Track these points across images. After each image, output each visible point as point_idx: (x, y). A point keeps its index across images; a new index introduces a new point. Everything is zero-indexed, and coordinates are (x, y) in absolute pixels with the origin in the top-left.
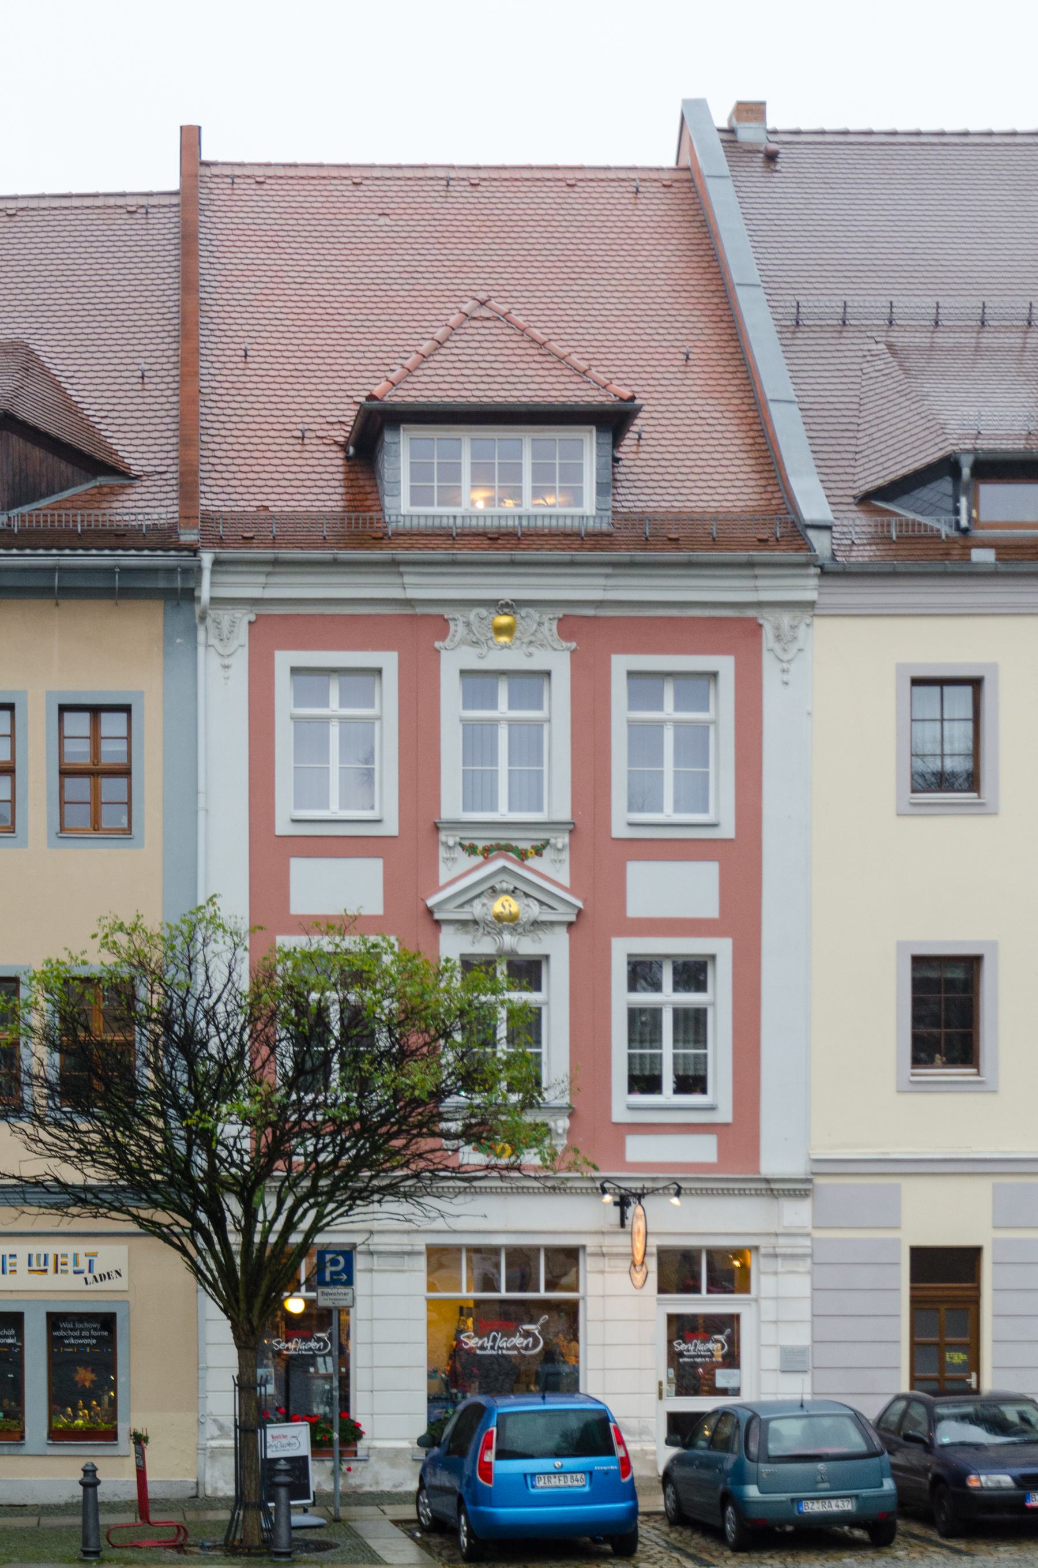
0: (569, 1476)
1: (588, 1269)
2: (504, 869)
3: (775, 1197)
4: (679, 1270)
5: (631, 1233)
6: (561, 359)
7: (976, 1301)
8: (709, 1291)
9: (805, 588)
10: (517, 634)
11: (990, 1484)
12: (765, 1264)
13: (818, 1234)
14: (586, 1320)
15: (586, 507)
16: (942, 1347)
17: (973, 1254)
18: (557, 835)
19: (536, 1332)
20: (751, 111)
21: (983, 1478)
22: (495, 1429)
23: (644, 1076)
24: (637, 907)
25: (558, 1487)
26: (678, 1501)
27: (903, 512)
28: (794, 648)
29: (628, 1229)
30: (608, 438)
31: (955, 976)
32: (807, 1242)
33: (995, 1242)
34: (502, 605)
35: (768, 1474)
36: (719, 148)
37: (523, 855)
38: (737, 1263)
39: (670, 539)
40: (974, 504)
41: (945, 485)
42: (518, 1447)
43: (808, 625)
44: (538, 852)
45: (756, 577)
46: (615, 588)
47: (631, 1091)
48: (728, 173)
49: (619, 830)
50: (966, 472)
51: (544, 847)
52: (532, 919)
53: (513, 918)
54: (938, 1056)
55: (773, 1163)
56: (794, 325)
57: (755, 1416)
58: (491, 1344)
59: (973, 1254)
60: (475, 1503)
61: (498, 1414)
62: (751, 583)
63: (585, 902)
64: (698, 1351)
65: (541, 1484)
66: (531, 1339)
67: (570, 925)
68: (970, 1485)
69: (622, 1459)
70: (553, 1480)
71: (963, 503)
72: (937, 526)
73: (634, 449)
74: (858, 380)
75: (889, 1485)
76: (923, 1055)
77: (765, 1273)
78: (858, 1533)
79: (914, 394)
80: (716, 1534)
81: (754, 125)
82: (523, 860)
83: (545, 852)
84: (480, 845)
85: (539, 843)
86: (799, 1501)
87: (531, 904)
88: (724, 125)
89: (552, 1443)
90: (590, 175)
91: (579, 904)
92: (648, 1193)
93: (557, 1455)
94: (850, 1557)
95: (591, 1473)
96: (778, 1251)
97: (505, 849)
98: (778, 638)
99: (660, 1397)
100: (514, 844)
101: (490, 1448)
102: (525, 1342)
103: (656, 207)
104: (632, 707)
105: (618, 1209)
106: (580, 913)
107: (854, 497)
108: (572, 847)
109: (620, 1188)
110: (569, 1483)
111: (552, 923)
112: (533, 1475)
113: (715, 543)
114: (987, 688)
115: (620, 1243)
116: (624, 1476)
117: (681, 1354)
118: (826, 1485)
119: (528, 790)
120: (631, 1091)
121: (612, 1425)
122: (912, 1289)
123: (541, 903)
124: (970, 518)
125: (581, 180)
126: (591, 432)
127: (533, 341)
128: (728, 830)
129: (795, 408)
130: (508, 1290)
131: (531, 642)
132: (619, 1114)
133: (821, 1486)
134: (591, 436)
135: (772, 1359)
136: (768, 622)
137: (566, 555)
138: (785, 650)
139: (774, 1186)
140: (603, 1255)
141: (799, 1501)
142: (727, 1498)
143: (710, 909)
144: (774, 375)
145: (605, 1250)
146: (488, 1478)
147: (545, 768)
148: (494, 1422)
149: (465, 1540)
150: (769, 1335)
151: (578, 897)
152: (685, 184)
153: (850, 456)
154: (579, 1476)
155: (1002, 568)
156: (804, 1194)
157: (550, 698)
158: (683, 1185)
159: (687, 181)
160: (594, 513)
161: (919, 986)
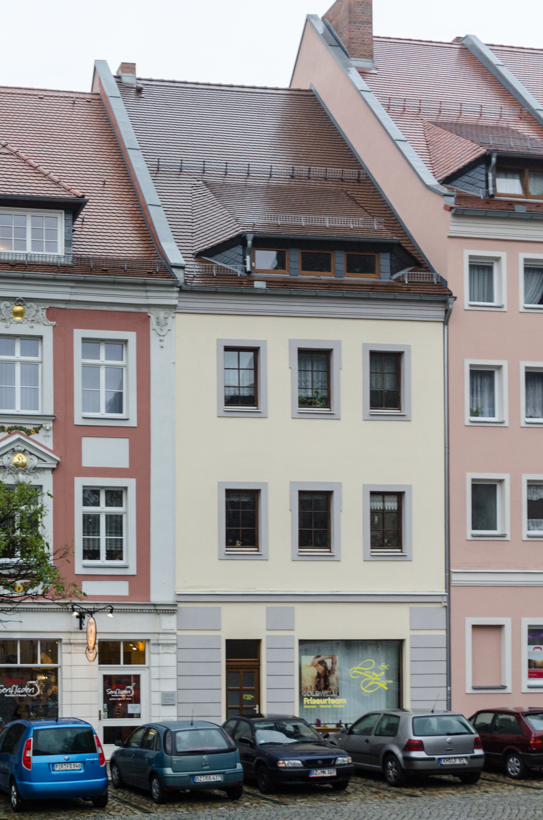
0: (72, 764)
1: (63, 651)
2: (19, 440)
3: (158, 614)
4: (108, 652)
5: (86, 632)
6: (46, 175)
7: (257, 668)
8: (124, 663)
9: (171, 298)
10: (25, 316)
11: (290, 765)
12: (153, 649)
13: (180, 633)
14: (62, 678)
15: (58, 252)
16: (241, 692)
17: (258, 642)
18: (47, 422)
19: (36, 685)
20: (128, 67)
21: (286, 762)
22: (32, 738)
23: (90, 550)
24: (88, 461)
25: (66, 770)
26: (120, 775)
27: (217, 262)
28: (166, 328)
29: (84, 630)
30: (70, 217)
31: (246, 500)
32: (174, 637)
33: (268, 637)
34: (18, 300)
35: (177, 761)
36: (115, 85)
37: (29, 433)
38: (134, 649)
39: (103, 270)
40: (253, 260)
41: (239, 250)
42: (44, 749)
43: (173, 317)
44: (37, 431)
45: (147, 291)
46: (76, 294)
47: (84, 558)
48: (120, 95)
49: (78, 421)
50: (249, 243)
51: (39, 428)
52: (34, 466)
53: (24, 465)
54: (238, 541)
55: (158, 595)
56: (156, 171)
57: (168, 730)
58: (12, 691)
59: (258, 642)
60: (22, 779)
61: (34, 730)
62: (144, 294)
63: (61, 457)
64: (119, 694)
65: (58, 769)
66: (33, 689)
67: (53, 470)
68: (280, 766)
69: (100, 754)
70: (64, 766)
71: (248, 258)
72: (235, 270)
73: (80, 226)
74: (190, 198)
75: (239, 766)
76: (230, 541)
77: (153, 653)
78: (216, 792)
79: (220, 205)
80: (147, 794)
81: (130, 75)
82: (29, 435)
83: (40, 431)
84: (7, 426)
85: (37, 426)
86: (193, 776)
87: (33, 458)
88: (115, 74)
89: (59, 746)
90: (50, 94)
91: (58, 459)
92: (97, 611)
93: (66, 753)
94: (222, 806)
95: (84, 762)
96: (160, 642)
97: (19, 429)
98: (158, 323)
99: (100, 719)
100: (24, 426)
101: (29, 749)
102: (30, 690)
103: (82, 112)
104: (83, 357)
105: (78, 620)
106: (58, 464)
107: (193, 254)
108: (54, 428)
109: (82, 608)
110: (73, 768)
111: (44, 469)
112: (53, 764)
113: (126, 273)
114: (262, 352)
115: (80, 637)
116: (102, 764)
117: (110, 696)
118: (208, 767)
119: (31, 397)
120: (84, 558)
121: (94, 735)
122: (227, 661)
123: (39, 458)
124: (252, 267)
125: (46, 96)
126: (61, 213)
127: (31, 166)
128: (133, 422)
129: (161, 209)
130: (21, 663)
131: (33, 321)
132: (79, 570)
133: (205, 768)
134: (62, 216)
135: (157, 698)
136: (153, 314)
137: (51, 275)
138: (161, 330)
139: (158, 608)
140: (71, 644)
141: (193, 776)
142: (154, 774)
143: (124, 463)
144: (149, 192)
145: (72, 641)
146: (28, 766)
147: (40, 387)
148: (32, 734)
149: (15, 800)
150: (155, 685)
151: (57, 456)
152: (97, 102)
153: (190, 234)
154: (78, 764)
155: (269, 292)
156: (173, 612)
157: (42, 350)
158: (115, 607)
159: (98, 100)
160: (63, 255)
161: (230, 505)
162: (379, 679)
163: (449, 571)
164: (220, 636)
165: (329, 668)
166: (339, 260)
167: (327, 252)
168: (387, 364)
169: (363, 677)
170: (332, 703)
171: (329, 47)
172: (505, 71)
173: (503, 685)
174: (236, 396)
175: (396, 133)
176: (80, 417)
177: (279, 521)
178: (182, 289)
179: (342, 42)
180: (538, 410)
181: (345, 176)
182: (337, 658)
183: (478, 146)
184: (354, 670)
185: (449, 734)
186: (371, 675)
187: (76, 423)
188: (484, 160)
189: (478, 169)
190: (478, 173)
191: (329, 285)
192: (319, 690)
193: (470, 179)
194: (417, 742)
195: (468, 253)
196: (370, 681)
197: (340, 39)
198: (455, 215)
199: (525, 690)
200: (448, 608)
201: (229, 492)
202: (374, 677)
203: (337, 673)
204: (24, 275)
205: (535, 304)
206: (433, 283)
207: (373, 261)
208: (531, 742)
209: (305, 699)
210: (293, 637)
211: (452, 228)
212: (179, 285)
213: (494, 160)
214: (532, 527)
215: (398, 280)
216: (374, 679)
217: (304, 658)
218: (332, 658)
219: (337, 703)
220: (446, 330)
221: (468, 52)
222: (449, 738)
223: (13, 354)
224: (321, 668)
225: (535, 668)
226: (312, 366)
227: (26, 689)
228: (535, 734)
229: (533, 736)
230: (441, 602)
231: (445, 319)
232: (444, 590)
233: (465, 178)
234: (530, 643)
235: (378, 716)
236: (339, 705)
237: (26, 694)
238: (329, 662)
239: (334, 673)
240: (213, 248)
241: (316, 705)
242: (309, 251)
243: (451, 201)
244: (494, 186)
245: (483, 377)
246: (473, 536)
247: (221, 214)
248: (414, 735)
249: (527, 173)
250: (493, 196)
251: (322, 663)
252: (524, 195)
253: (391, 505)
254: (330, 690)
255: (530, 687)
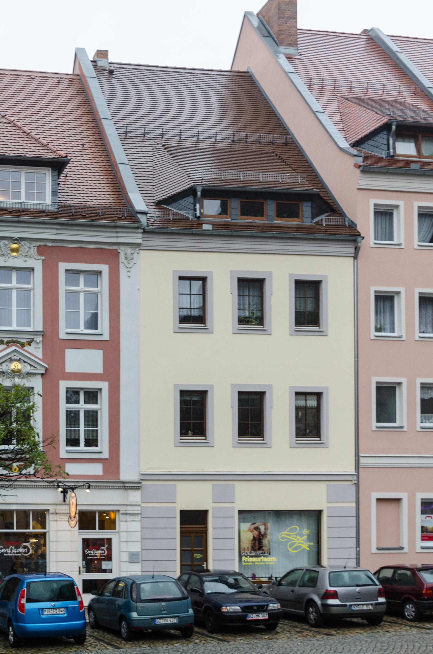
0: (58, 609)
1: (51, 519)
2: (15, 351)
3: (126, 489)
4: (86, 520)
5: (69, 504)
6: (36, 140)
7: (205, 532)
8: (99, 529)
9: (137, 238)
10: (20, 252)
11: (231, 610)
12: (122, 517)
13: (143, 505)
14: (49, 541)
15: (47, 201)
16: (192, 552)
17: (206, 512)
18: (37, 337)
19: (29, 546)
20: (102, 54)
21: (228, 608)
22: (25, 589)
23: (71, 439)
24: (70, 368)
25: (53, 614)
26: (95, 618)
27: (173, 209)
28: (132, 262)
29: (67, 503)
30: (56, 173)
31: (196, 399)
32: (139, 508)
33: (213, 508)
34: (14, 239)
35: (141, 607)
36: (92, 67)
37: (23, 345)
38: (107, 517)
39: (82, 215)
40: (202, 207)
41: (190, 199)
42: (35, 598)
43: (138, 253)
44: (29, 344)
45: (117, 232)
46: (60, 234)
47: (67, 445)
48: (95, 76)
49: (62, 336)
50: (199, 193)
51: (31, 342)
52: (27, 372)
53: (19, 371)
54: (190, 432)
55: (126, 475)
56: (125, 136)
57: (134, 582)
58: (10, 551)
59: (206, 512)
60: (17, 622)
61: (27, 582)
62: (115, 235)
63: (48, 365)
64: (95, 553)
65: (46, 613)
66: (26, 549)
67: (42, 375)
68: (223, 611)
69: (80, 601)
70: (51, 611)
71: (198, 206)
72: (187, 215)
73: (64, 180)
74: (152, 158)
75: (191, 611)
76: (184, 431)
77: (122, 521)
78: (173, 631)
79: (175, 163)
80: (117, 633)
81: (104, 60)
82: (23, 347)
83: (32, 344)
84: (5, 340)
85: (29, 340)
86: (154, 619)
87: (26, 366)
88: (92, 59)
89: (47, 595)
90: (40, 75)
91: (46, 366)
92: (77, 487)
93: (53, 601)
94: (177, 643)
95: (67, 608)
96: (128, 512)
97: (15, 342)
98: (126, 258)
99: (80, 574)
100: (19, 340)
101: (23, 597)
102: (24, 550)
103: (66, 90)
104: (67, 285)
105: (62, 494)
106: (46, 370)
107: (154, 203)
108: (43, 341)
109: (66, 485)
110: (58, 613)
111: (35, 374)
112: (42, 609)
113: (100, 218)
114: (209, 281)
115: (64, 508)
116: (81, 609)
117: (88, 555)
118: (166, 612)
119: (25, 317)
120: (67, 445)
121: (75, 587)
122: (181, 527)
123: (31, 365)
124: (201, 213)
125: (36, 76)
126: (49, 170)
127: (25, 132)
128: (106, 337)
129: (129, 167)
130: (17, 529)
131: (26, 256)
132: (63, 454)
133: (163, 612)
134: (49, 172)
135: (125, 557)
136: (122, 251)
137: (40, 220)
138: (129, 263)
139: (126, 485)
140: (57, 514)
141: (154, 619)
142: (123, 618)
143: (99, 369)
144: (119, 153)
145: (57, 511)
146: (23, 611)
147: (32, 309)
148: (25, 585)
149: (12, 638)
150: (124, 547)
151: (46, 363)
152: (78, 81)
153: (152, 187)
154: (62, 609)
155: (215, 233)
156: (138, 488)
157: (34, 279)
158: (91, 484)
159: (78, 79)
160: (51, 203)
161: (183, 403)
162: (302, 542)
163: (358, 455)
164: (175, 507)
165: (263, 533)
166: (270, 207)
167: (261, 201)
168: (308, 291)
169: (290, 540)
170: (265, 561)
171: (263, 38)
172: (403, 57)
173: (401, 546)
174: (188, 316)
175: (316, 106)
176: (64, 333)
177: (222, 415)
178: (145, 231)
179: (272, 34)
180: (429, 327)
181: (275, 141)
182: (269, 525)
183: (381, 116)
184: (282, 534)
185: (358, 586)
186: (296, 538)
187: (60, 337)
188: (386, 127)
189: (381, 135)
190: (381, 138)
191: (262, 227)
192: (254, 551)
193: (375, 142)
194: (332, 592)
195: (373, 201)
196: (295, 543)
197: (271, 31)
198: (363, 172)
199: (419, 550)
200: (357, 485)
201: (183, 393)
202: (298, 540)
203: (269, 537)
204: (19, 219)
205: (426, 242)
206: (346, 226)
207: (297, 208)
208: (424, 592)
209: (243, 557)
210: (233, 508)
211: (360, 182)
212: (143, 228)
213: (394, 127)
214: (424, 421)
215: (317, 223)
216: (298, 541)
217: (242, 525)
218: (265, 525)
219: (269, 561)
220: (356, 263)
221: (373, 42)
222: (358, 589)
223: (10, 282)
224: (256, 533)
225: (427, 533)
226: (249, 292)
227: (21, 550)
228: (426, 585)
229: (425, 587)
230: (352, 480)
231: (355, 254)
232: (354, 471)
233: (371, 142)
234: (423, 513)
235: (301, 571)
236: (270, 562)
237: (21, 553)
238: (262, 528)
239: (266, 537)
240: (170, 197)
241: (252, 562)
242: (246, 200)
243: (360, 160)
244: (394, 148)
245: (385, 301)
246: (377, 427)
247: (176, 170)
248: (330, 586)
249: (420, 138)
250: (393, 156)
251: (257, 528)
252: (418, 156)
253: (312, 403)
254: (263, 550)
255: (422, 548)
